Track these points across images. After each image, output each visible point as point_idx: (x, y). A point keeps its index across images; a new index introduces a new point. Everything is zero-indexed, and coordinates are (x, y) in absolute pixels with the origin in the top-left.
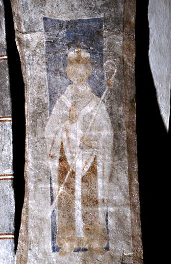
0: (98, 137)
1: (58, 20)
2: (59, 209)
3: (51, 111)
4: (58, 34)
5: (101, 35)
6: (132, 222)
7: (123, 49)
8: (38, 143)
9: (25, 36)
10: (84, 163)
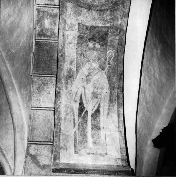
0: (101, 93)
1: (86, 25)
2: (78, 131)
3: (76, 76)
4: (85, 33)
5: (108, 36)
6: (120, 141)
7: (118, 45)
8: (68, 93)
9: (67, 32)
10: (93, 107)
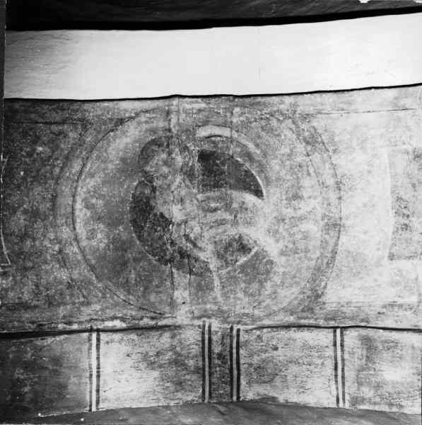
1: (393, 233)
